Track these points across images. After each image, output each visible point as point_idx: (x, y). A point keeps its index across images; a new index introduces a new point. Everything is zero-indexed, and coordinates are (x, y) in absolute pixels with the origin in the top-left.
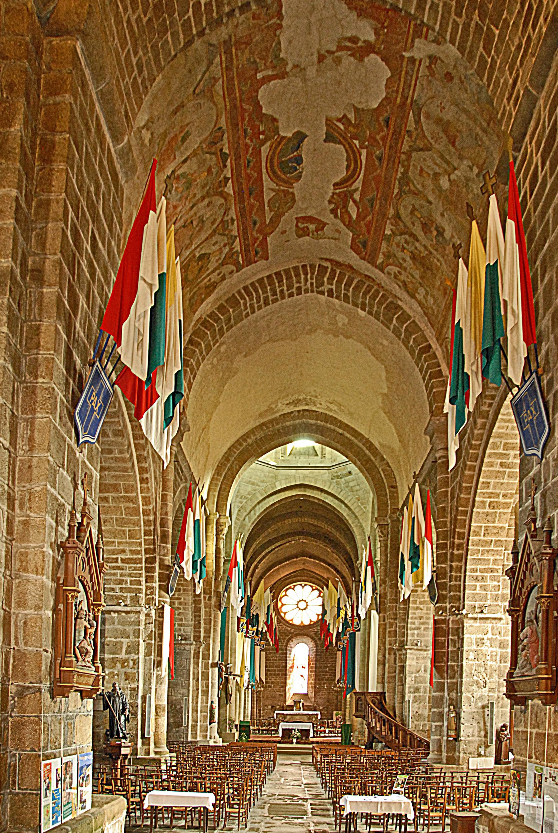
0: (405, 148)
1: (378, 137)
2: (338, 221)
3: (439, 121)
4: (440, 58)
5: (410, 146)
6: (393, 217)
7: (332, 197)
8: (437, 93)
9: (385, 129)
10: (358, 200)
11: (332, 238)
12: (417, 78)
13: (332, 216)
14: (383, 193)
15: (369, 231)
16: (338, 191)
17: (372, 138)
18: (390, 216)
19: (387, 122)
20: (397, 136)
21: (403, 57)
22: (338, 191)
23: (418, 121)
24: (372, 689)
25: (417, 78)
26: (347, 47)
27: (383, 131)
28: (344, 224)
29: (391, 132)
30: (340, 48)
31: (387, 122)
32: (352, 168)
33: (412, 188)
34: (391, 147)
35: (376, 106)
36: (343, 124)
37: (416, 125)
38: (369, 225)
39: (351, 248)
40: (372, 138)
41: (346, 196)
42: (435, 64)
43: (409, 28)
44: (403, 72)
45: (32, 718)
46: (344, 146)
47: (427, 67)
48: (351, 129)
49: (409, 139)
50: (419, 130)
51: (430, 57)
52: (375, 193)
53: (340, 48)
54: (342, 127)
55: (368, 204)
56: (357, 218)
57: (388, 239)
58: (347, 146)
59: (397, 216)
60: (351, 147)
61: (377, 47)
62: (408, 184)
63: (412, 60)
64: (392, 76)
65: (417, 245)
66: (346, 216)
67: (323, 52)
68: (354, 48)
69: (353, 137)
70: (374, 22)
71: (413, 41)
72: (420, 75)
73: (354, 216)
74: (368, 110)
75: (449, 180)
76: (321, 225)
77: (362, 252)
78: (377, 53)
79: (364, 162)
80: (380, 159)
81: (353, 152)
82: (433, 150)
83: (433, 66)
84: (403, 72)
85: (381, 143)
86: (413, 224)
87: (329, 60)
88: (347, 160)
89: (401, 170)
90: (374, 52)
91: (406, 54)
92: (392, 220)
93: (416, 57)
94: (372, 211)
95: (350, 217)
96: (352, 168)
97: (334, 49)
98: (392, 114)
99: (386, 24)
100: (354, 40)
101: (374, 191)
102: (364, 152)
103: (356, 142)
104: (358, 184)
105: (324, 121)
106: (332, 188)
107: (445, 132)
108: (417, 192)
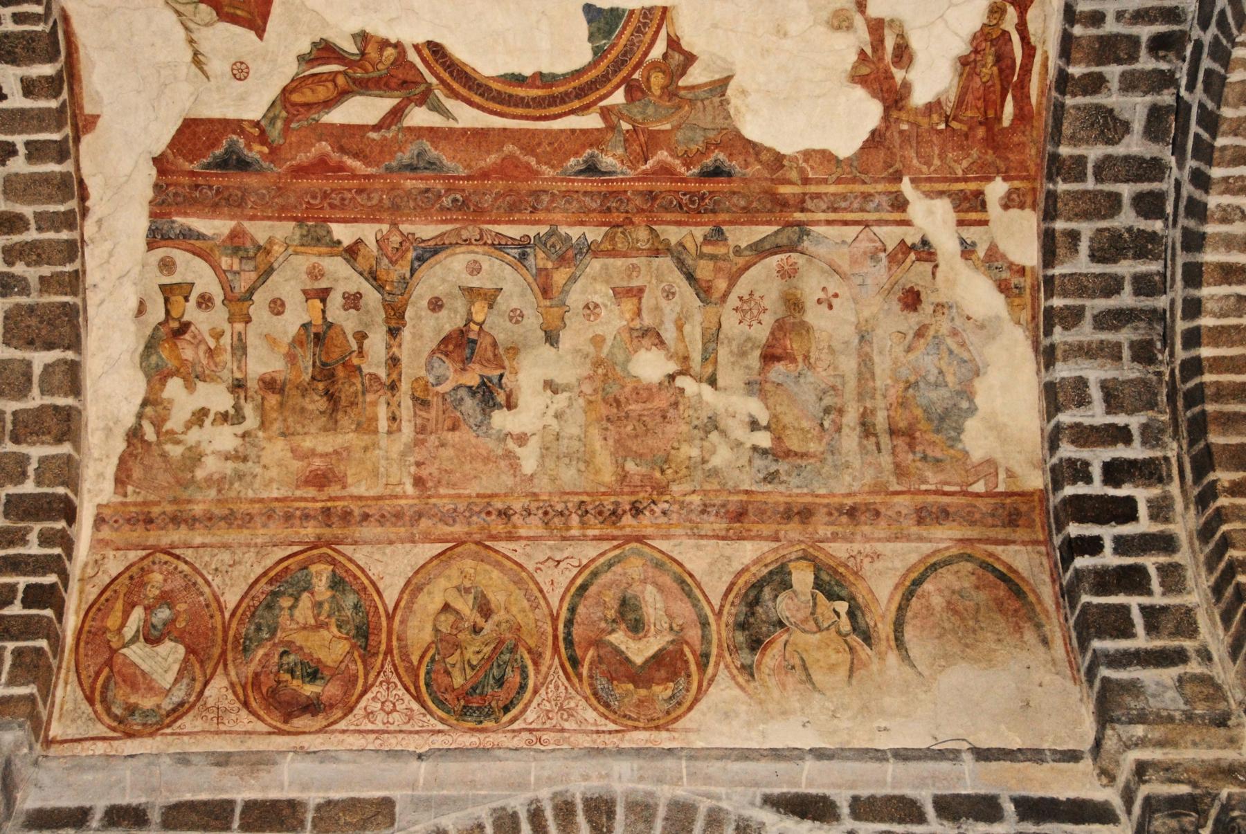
0: (673, 234)
1: (663, 155)
2: (289, 70)
3: (794, 304)
4: (936, 266)
5: (681, 244)
7: (385, 44)
8: (859, 281)
9: (695, 170)
12: (867, 225)
17: (653, 141)
18: (406, 228)
21: (900, 180)
23: (760, 250)
25: (867, 225)
26: (882, 41)
27: (687, 165)
29: (692, 186)
30: (877, 28)
31: (717, 172)
32: (520, 92)
36: (665, 56)
37: (750, 246)
40: (653, 141)
42: (918, 260)
43: (966, 180)
44: (863, 188)
46: (593, 64)
47: (903, 242)
48: (657, 80)
49: (700, 239)
50: (741, 261)
51: (925, 242)
52: (463, 172)
53: (877, 28)
55: (406, 156)
57: (317, 239)
58: (593, 74)
59: (429, 252)
60: (604, 79)
61: (903, 115)
63: (900, 204)
64: (838, 161)
65: (377, 342)
66: (323, 93)
68: (881, 59)
69: (633, 91)
70: (953, 97)
71: (941, 194)
72: (875, 229)
73: (338, 116)
74: (728, 116)
75: (672, 377)
77: (192, 156)
78: (886, 117)
80: (591, 169)
81: (581, 92)
82: (711, 309)
83: (913, 256)
84: (863, 188)
86: (436, 305)
89: (594, 234)
90: (887, 110)
93: (910, 209)
94: (389, 169)
95: (329, 104)
96: (520, 92)
98: (744, 179)
99: (954, 125)
100: (903, 54)
101: (468, 166)
102: (592, 121)
103: (618, 97)
104: (467, 116)
106: (421, 39)
107: (780, 327)
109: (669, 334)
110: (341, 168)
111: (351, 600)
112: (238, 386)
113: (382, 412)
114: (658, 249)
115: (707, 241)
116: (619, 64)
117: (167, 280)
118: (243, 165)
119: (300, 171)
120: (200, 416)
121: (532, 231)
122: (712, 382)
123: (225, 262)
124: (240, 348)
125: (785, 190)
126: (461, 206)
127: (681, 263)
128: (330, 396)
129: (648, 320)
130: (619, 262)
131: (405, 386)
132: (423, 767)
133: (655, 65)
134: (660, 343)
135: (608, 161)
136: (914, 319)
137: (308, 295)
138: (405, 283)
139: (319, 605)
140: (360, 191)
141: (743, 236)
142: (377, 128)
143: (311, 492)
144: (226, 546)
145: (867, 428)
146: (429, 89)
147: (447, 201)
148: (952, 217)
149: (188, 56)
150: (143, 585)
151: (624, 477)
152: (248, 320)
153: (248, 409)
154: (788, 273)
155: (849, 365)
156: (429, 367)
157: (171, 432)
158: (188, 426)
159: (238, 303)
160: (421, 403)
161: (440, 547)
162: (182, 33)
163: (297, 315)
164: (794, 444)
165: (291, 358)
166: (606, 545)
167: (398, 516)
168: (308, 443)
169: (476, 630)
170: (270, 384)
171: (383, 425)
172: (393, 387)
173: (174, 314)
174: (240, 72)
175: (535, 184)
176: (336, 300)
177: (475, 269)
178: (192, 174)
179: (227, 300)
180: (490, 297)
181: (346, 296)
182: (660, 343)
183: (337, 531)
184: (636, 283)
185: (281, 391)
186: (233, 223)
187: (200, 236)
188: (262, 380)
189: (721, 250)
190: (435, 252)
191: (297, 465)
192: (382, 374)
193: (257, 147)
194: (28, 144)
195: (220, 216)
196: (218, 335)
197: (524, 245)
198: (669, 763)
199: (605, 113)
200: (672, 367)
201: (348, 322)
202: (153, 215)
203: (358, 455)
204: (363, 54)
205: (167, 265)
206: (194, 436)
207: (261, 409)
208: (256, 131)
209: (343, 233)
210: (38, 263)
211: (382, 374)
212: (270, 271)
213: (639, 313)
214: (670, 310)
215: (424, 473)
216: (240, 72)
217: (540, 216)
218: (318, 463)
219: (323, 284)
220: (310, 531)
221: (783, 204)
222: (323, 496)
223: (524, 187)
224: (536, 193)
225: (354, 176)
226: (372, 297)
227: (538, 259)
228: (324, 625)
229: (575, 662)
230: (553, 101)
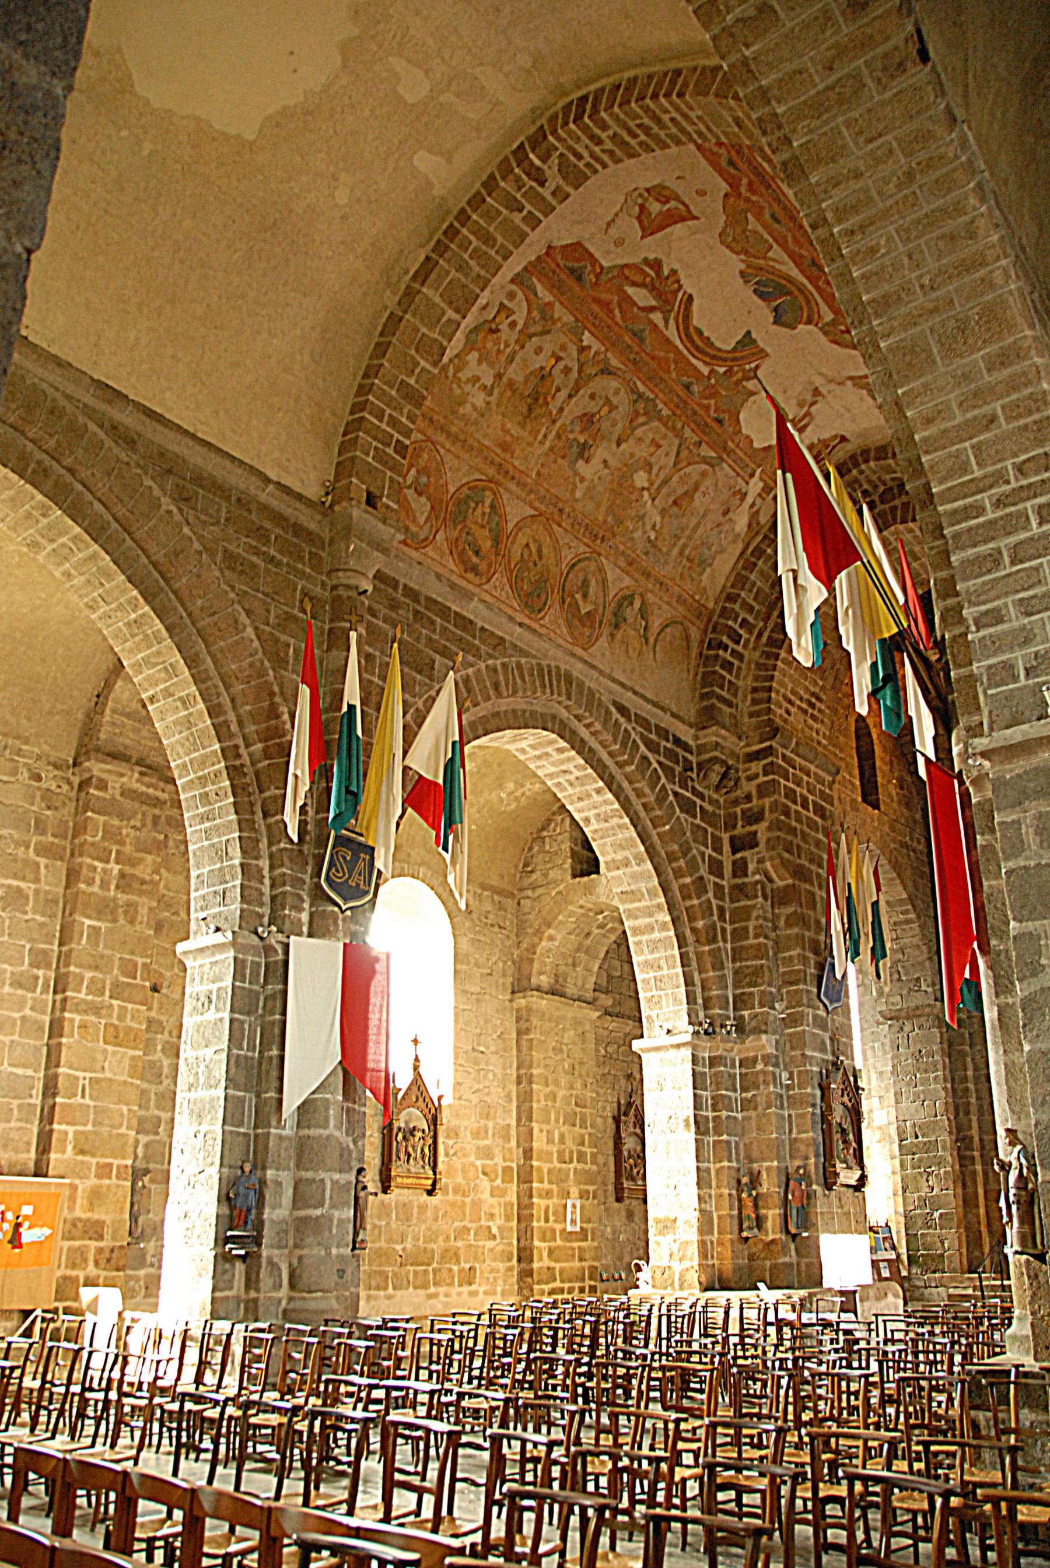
2: (637, 259)
6: (606, 360)
7: (678, 281)
10: (652, 316)
11: (613, 220)
12: (738, 475)
13: (652, 257)
14: (646, 364)
15: (598, 301)
16: (680, 295)
17: (715, 395)
18: (609, 355)
19: (720, 422)
20: (703, 428)
22: (680, 295)
23: (705, 460)
24: (464, 1456)
25: (738, 475)
28: (626, 265)
31: (720, 422)
32: (696, 338)
33: (641, 420)
34: (695, 413)
35: (741, 417)
38: (606, 305)
39: (579, 244)
40: (715, 395)
41: (666, 301)
45: (121, 511)
46: (729, 352)
52: (648, 350)
54: (747, 367)
56: (625, 293)
57: (576, 334)
58: (724, 355)
59: (607, 371)
62: (646, 414)
65: (563, 395)
67: (819, 398)
69: (729, 372)
73: (630, 290)
75: (643, 489)
76: (650, 227)
79: (694, 361)
80: (687, 387)
81: (713, 357)
85: (705, 402)
87: (809, 398)
88: (708, 339)
89: (665, 412)
91: (759, 471)
92: (602, 356)
95: (634, 284)
96: (696, 338)
97: (813, 410)
104: (672, 333)
105: (769, 350)
106: (689, 291)
108: (635, 424)
109: (655, 471)
110: (611, 311)
111: (497, 519)
112: (499, 376)
113: (543, 431)
114: (679, 435)
115: (695, 444)
116: (735, 359)
117: (506, 302)
118: (579, 279)
119: (598, 301)
120: (476, 379)
121: (648, 393)
122: (653, 500)
123: (535, 313)
124: (511, 360)
125: (730, 444)
126: (635, 363)
127: (680, 445)
128: (530, 410)
129: (653, 460)
130: (663, 429)
131: (558, 424)
132: (519, 630)
133: (744, 371)
134: (650, 473)
135: (695, 388)
136: (721, 519)
137: (553, 354)
138: (590, 378)
139: (484, 514)
140: (608, 327)
141: (706, 451)
142: (639, 308)
143: (499, 451)
144: (458, 457)
145: (681, 553)
146: (670, 311)
147: (632, 356)
148: (759, 490)
149: (609, 219)
150: (419, 456)
151: (605, 521)
152: (523, 347)
153: (496, 391)
154: (704, 474)
155: (693, 522)
156: (572, 422)
157: (459, 379)
158: (468, 381)
159: (526, 335)
160: (558, 436)
161: (534, 512)
162: (618, 208)
163: (543, 361)
164: (659, 544)
165: (527, 380)
166: (587, 549)
167: (525, 485)
168: (509, 426)
169: (535, 564)
170: (511, 384)
171: (540, 437)
172: (554, 422)
173: (497, 320)
174: (619, 243)
175: (666, 376)
176: (561, 365)
177: (617, 392)
178: (558, 266)
179: (521, 331)
180: (613, 408)
181: (566, 367)
182: (650, 473)
183: (500, 478)
184: (662, 442)
185: (514, 391)
186: (552, 299)
187: (536, 294)
188: (510, 380)
189: (695, 451)
190: (610, 374)
191: (500, 432)
192: (554, 412)
193: (592, 276)
194: (530, 212)
195: (551, 292)
196: (507, 346)
197: (641, 396)
198: (593, 672)
199: (712, 371)
200: (646, 485)
201: (558, 379)
202: (525, 269)
203: (524, 445)
204: (667, 278)
205: (511, 296)
206: (468, 388)
207: (502, 394)
208: (598, 270)
209: (587, 338)
210: (482, 267)
211: (554, 412)
212: (548, 332)
213: (651, 455)
214: (663, 461)
215: (543, 471)
216: (619, 243)
217: (656, 390)
218: (508, 438)
219: (562, 354)
220: (491, 472)
221: (725, 448)
222: (502, 455)
223: (661, 373)
224: (662, 380)
225: (613, 319)
226: (574, 375)
227: (641, 406)
228: (483, 526)
229: (564, 602)
230: (702, 352)
